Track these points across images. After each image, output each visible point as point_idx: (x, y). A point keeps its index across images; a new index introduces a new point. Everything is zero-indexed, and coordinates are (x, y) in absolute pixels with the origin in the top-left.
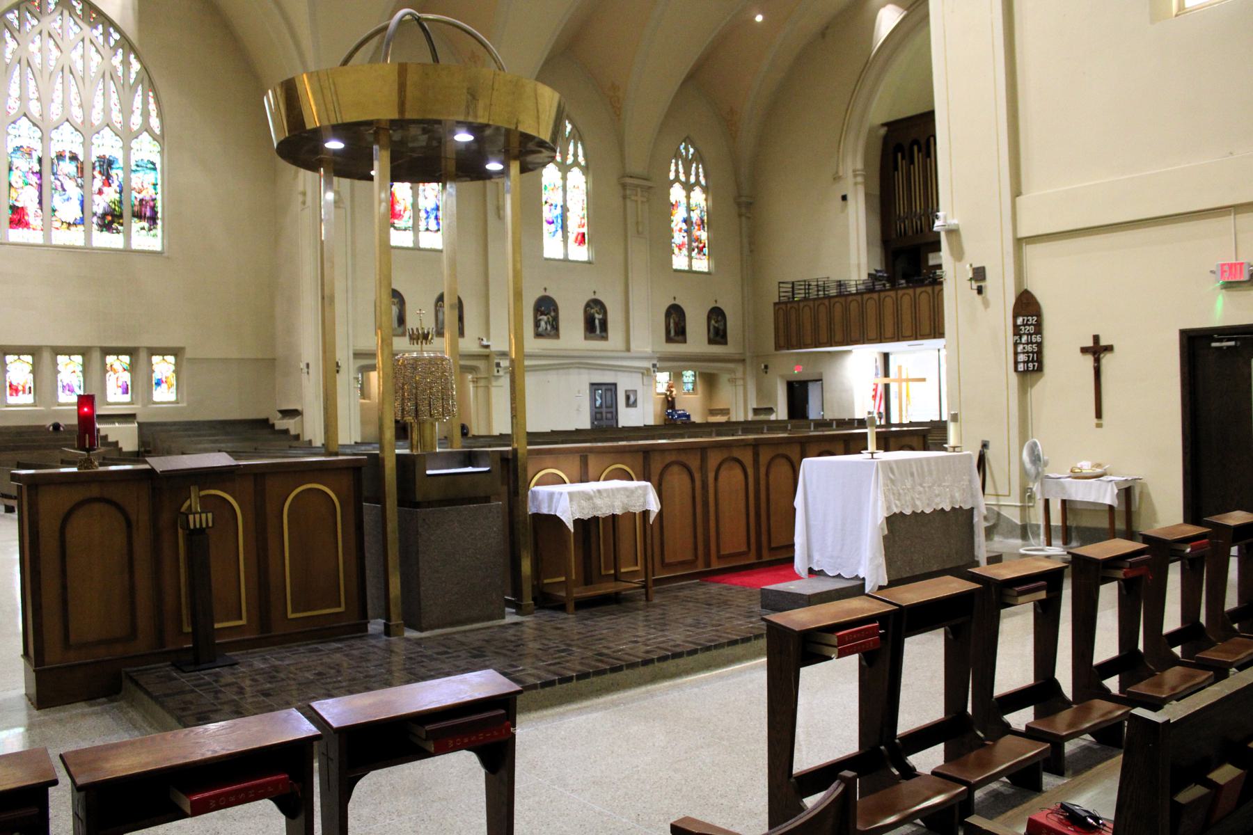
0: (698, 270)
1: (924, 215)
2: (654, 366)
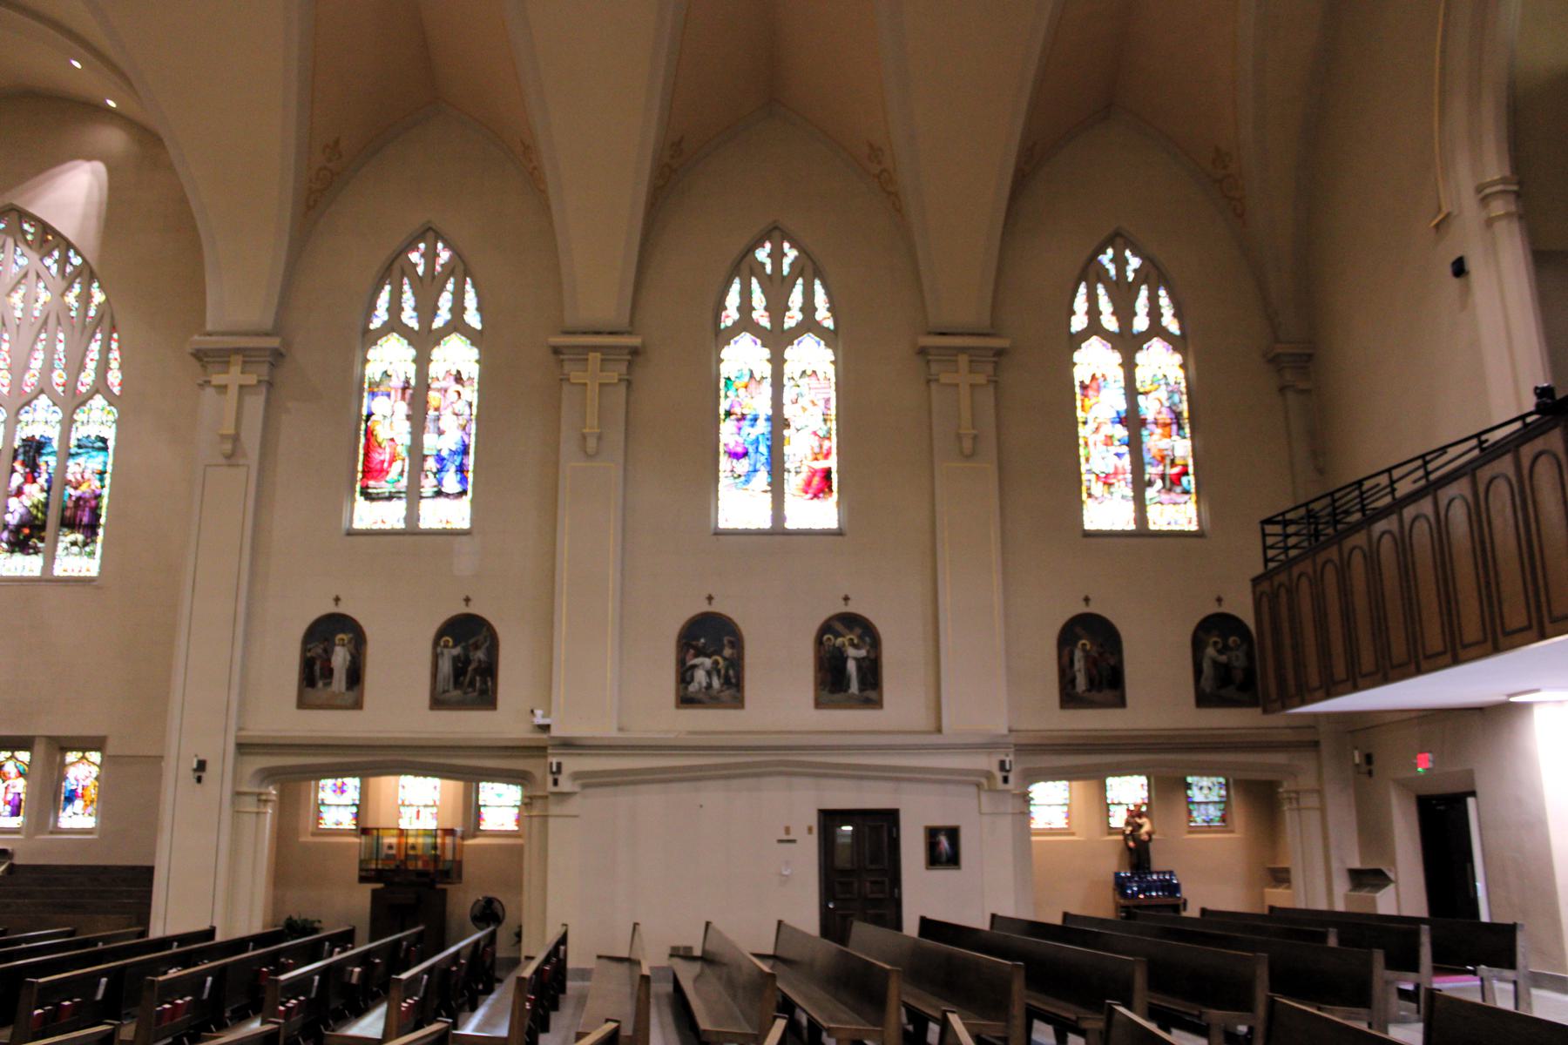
0: (1165, 528)
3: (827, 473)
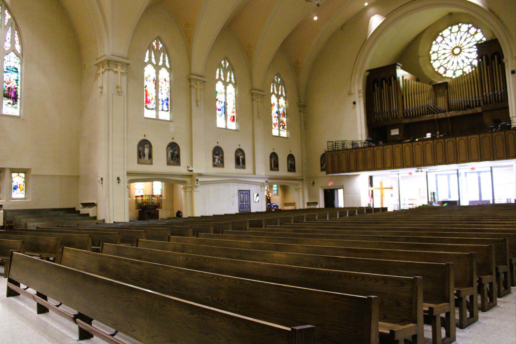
0: (282, 136)
1: (380, 113)
2: (267, 182)
3: (234, 117)
